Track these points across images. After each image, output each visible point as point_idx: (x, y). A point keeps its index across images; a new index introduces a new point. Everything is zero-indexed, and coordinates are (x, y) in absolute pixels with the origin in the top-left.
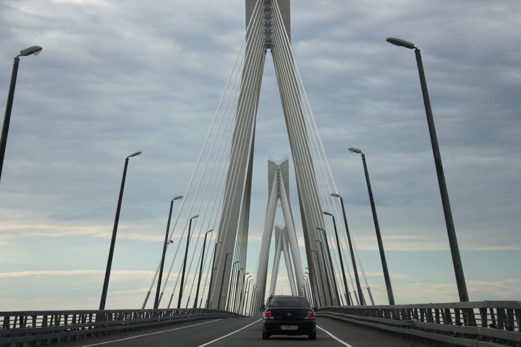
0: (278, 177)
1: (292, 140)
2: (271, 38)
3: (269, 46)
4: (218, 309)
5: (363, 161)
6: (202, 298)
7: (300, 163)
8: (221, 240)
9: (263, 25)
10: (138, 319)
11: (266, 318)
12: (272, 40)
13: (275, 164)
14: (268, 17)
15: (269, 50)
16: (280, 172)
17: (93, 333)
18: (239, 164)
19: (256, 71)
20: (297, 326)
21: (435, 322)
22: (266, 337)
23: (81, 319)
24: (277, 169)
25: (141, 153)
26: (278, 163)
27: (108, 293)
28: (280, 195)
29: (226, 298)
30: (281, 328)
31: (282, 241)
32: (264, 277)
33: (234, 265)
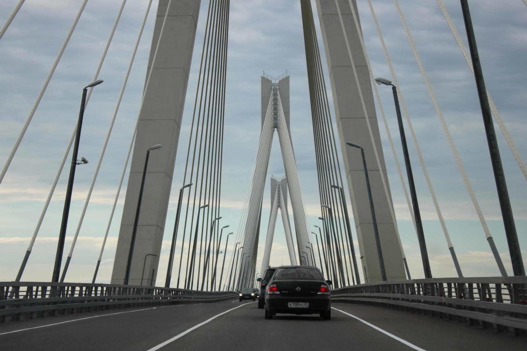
0: (275, 100)
3: (276, 127)
5: (393, 90)
10: (117, 295)
11: (271, 293)
13: (272, 82)
15: (279, 208)
16: (278, 93)
20: (308, 304)
23: (66, 292)
26: (275, 81)
28: (277, 125)
30: (288, 305)
31: (279, 197)
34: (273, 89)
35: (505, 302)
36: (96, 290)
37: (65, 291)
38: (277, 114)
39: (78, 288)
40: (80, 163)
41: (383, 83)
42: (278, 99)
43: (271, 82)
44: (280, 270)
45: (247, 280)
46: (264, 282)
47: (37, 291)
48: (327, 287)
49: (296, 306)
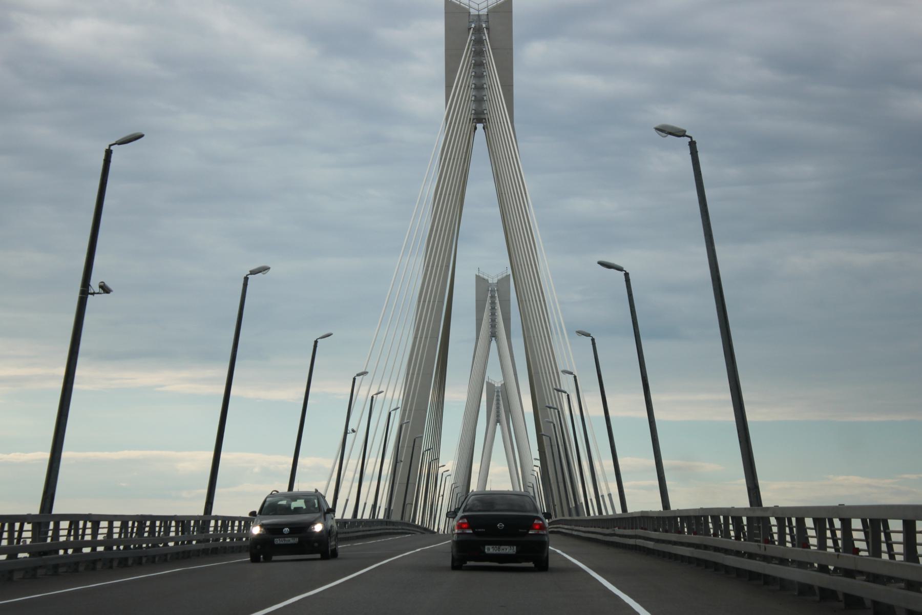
0: (493, 303)
1: (514, 265)
2: (484, 108)
3: (480, 121)
4: (401, 521)
7: (526, 301)
8: (407, 419)
9: (471, 89)
11: (459, 532)
12: (485, 112)
13: (488, 282)
14: (479, 76)
15: (480, 126)
16: (496, 295)
17: (146, 556)
18: (434, 302)
19: (461, 159)
20: (515, 547)
21: (777, 543)
22: (458, 565)
24: (497, 392)
25: (141, 136)
26: (493, 280)
27: (218, 491)
29: (412, 504)
31: (498, 408)
32: (468, 469)
33: (423, 453)
35: (812, 548)
36: (111, 527)
37: (164, 526)
38: (495, 314)
39: (104, 524)
40: (96, 292)
41: (670, 134)
44: (473, 497)
47: (84, 528)
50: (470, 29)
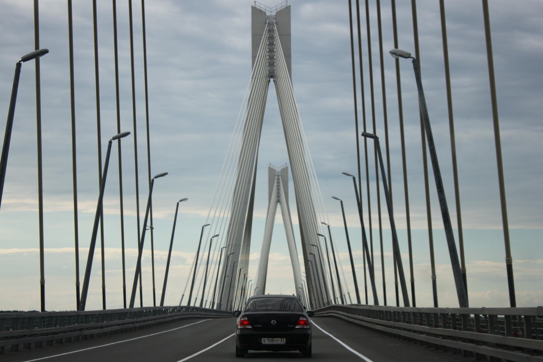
3: (272, 77)
6: (291, 304)
11: (241, 327)
13: (266, 15)
15: (272, 80)
16: (275, 28)
20: (285, 339)
22: (241, 353)
26: (278, 169)
28: (274, 73)
31: (278, 189)
34: (267, 23)
38: (273, 58)
42: (274, 37)
43: (265, 13)
45: (232, 289)
46: (236, 314)
48: (307, 320)
49: (271, 342)
50: (266, 23)
